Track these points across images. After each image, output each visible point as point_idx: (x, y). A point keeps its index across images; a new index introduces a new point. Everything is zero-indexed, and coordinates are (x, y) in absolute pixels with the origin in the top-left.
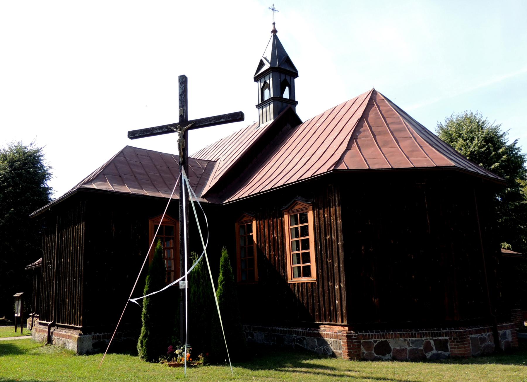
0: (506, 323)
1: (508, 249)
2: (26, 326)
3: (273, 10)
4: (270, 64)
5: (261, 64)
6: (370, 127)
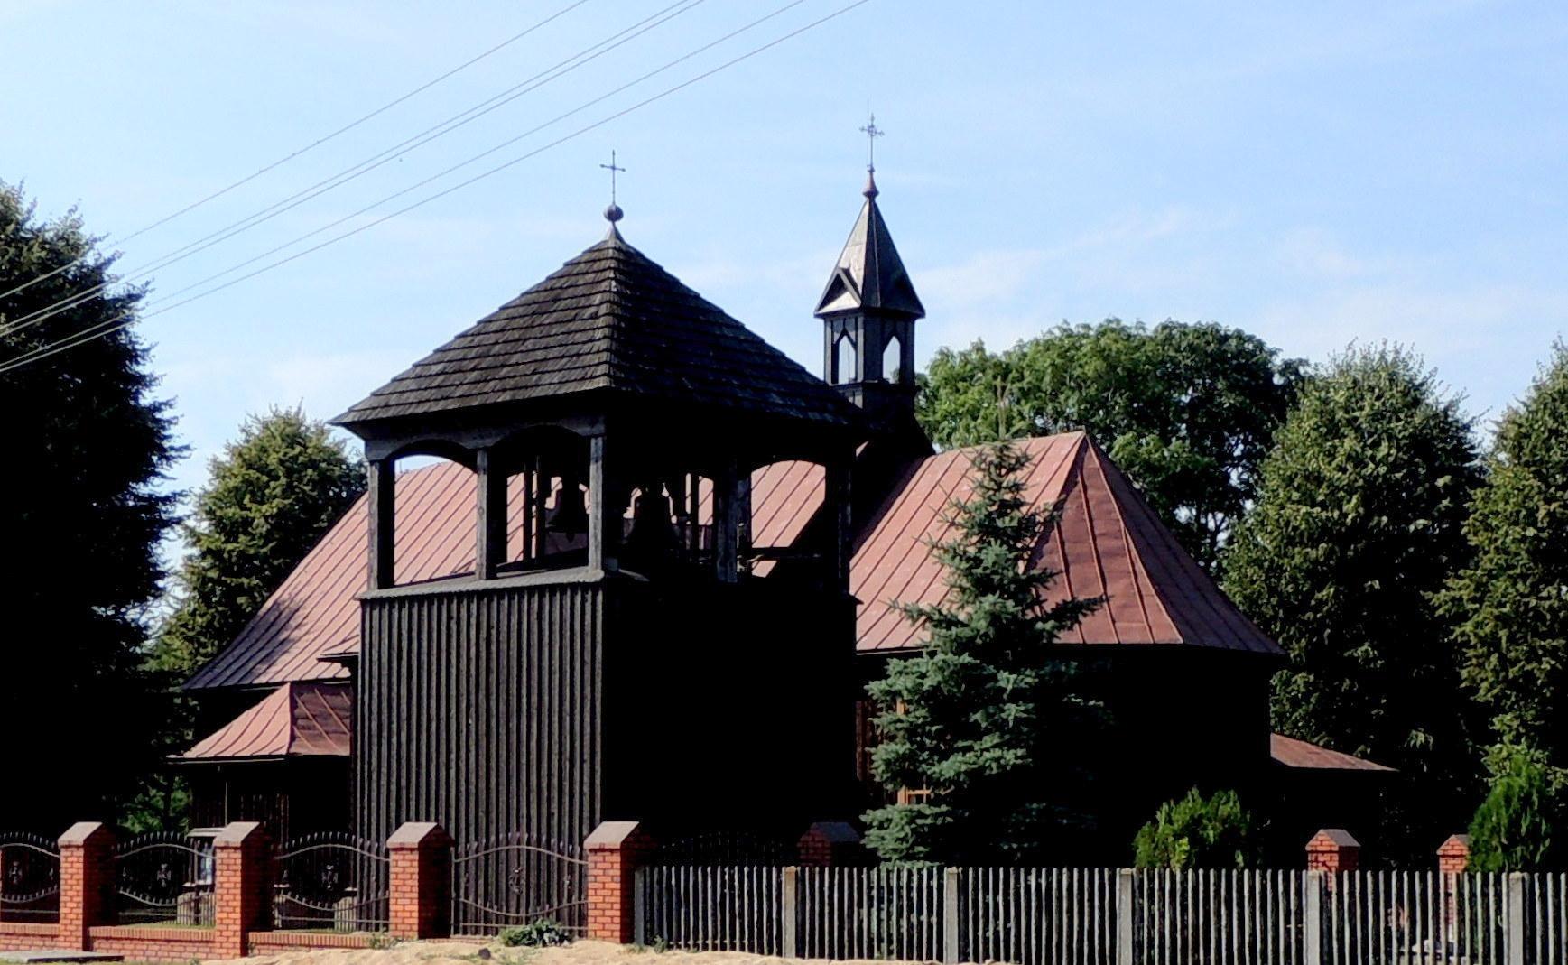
0: (153, 595)
1: (283, 928)
2: (54, 902)
3: (871, 130)
4: (862, 298)
5: (836, 288)
6: (1062, 543)
